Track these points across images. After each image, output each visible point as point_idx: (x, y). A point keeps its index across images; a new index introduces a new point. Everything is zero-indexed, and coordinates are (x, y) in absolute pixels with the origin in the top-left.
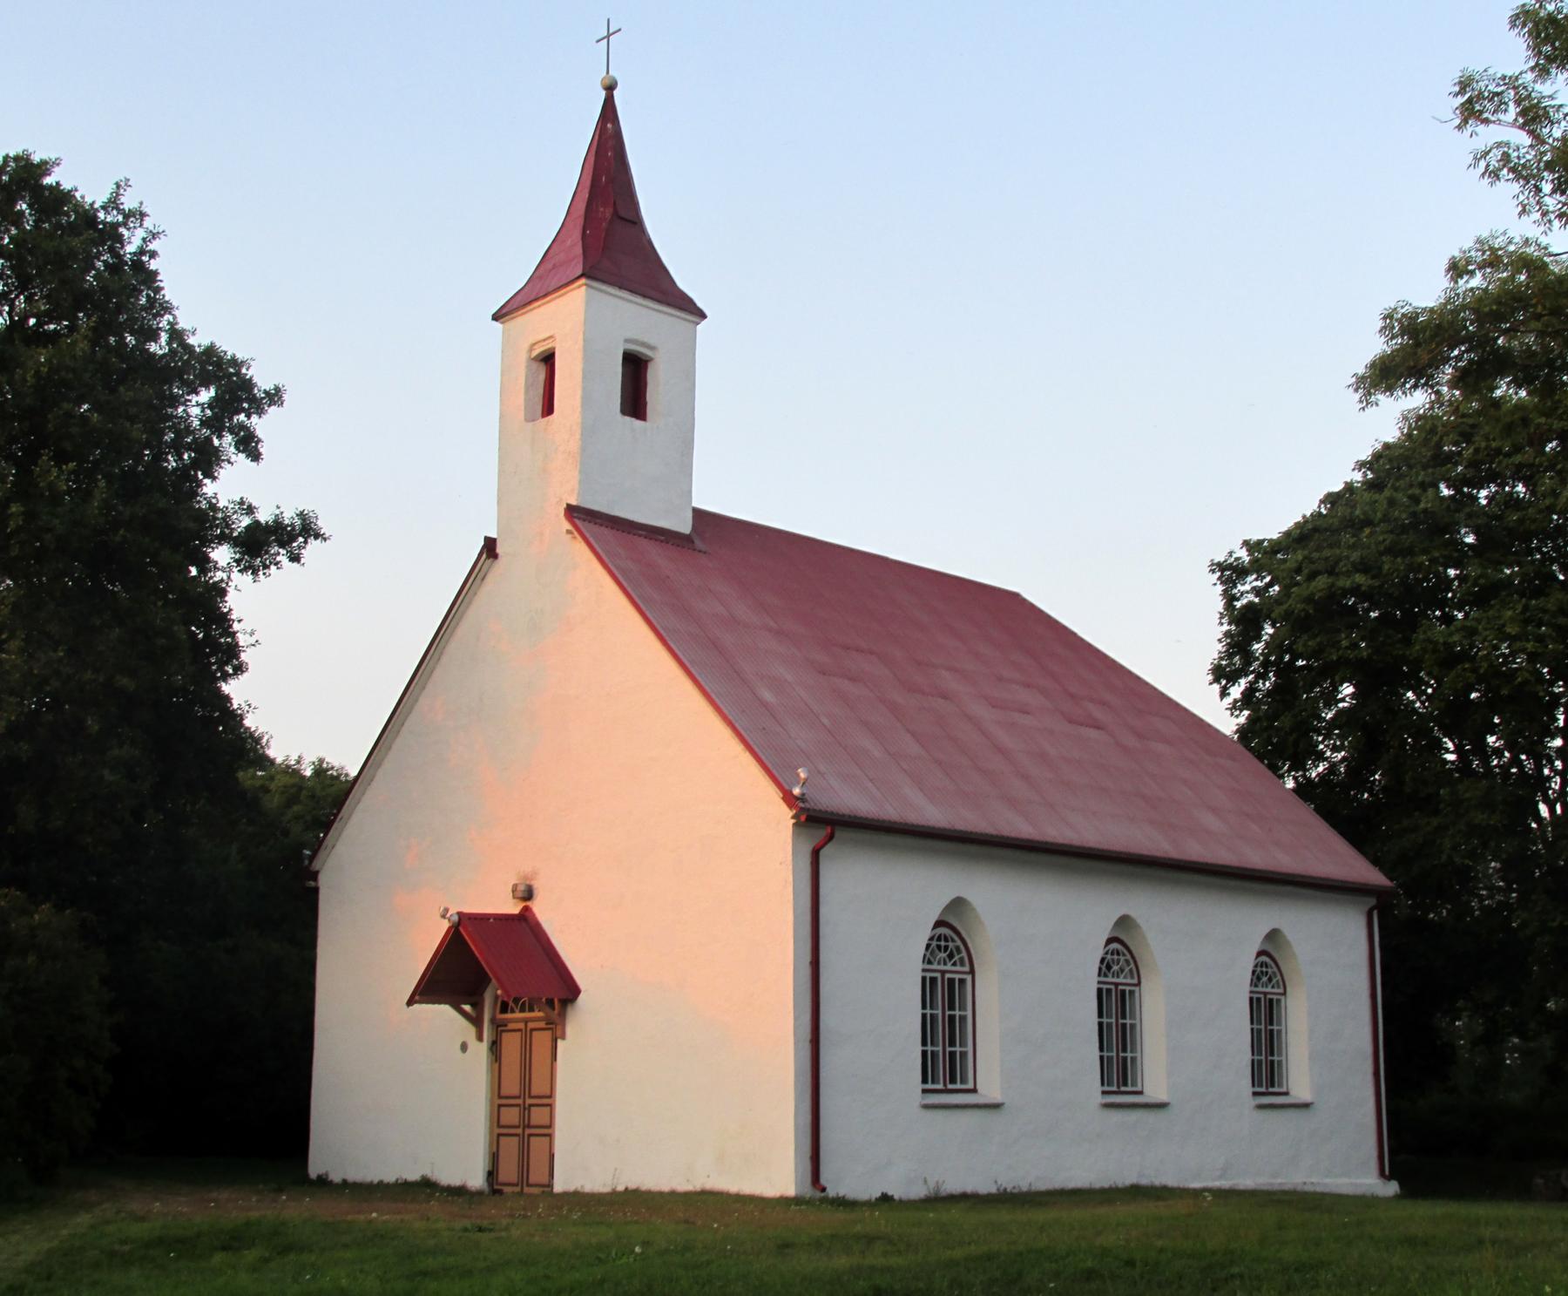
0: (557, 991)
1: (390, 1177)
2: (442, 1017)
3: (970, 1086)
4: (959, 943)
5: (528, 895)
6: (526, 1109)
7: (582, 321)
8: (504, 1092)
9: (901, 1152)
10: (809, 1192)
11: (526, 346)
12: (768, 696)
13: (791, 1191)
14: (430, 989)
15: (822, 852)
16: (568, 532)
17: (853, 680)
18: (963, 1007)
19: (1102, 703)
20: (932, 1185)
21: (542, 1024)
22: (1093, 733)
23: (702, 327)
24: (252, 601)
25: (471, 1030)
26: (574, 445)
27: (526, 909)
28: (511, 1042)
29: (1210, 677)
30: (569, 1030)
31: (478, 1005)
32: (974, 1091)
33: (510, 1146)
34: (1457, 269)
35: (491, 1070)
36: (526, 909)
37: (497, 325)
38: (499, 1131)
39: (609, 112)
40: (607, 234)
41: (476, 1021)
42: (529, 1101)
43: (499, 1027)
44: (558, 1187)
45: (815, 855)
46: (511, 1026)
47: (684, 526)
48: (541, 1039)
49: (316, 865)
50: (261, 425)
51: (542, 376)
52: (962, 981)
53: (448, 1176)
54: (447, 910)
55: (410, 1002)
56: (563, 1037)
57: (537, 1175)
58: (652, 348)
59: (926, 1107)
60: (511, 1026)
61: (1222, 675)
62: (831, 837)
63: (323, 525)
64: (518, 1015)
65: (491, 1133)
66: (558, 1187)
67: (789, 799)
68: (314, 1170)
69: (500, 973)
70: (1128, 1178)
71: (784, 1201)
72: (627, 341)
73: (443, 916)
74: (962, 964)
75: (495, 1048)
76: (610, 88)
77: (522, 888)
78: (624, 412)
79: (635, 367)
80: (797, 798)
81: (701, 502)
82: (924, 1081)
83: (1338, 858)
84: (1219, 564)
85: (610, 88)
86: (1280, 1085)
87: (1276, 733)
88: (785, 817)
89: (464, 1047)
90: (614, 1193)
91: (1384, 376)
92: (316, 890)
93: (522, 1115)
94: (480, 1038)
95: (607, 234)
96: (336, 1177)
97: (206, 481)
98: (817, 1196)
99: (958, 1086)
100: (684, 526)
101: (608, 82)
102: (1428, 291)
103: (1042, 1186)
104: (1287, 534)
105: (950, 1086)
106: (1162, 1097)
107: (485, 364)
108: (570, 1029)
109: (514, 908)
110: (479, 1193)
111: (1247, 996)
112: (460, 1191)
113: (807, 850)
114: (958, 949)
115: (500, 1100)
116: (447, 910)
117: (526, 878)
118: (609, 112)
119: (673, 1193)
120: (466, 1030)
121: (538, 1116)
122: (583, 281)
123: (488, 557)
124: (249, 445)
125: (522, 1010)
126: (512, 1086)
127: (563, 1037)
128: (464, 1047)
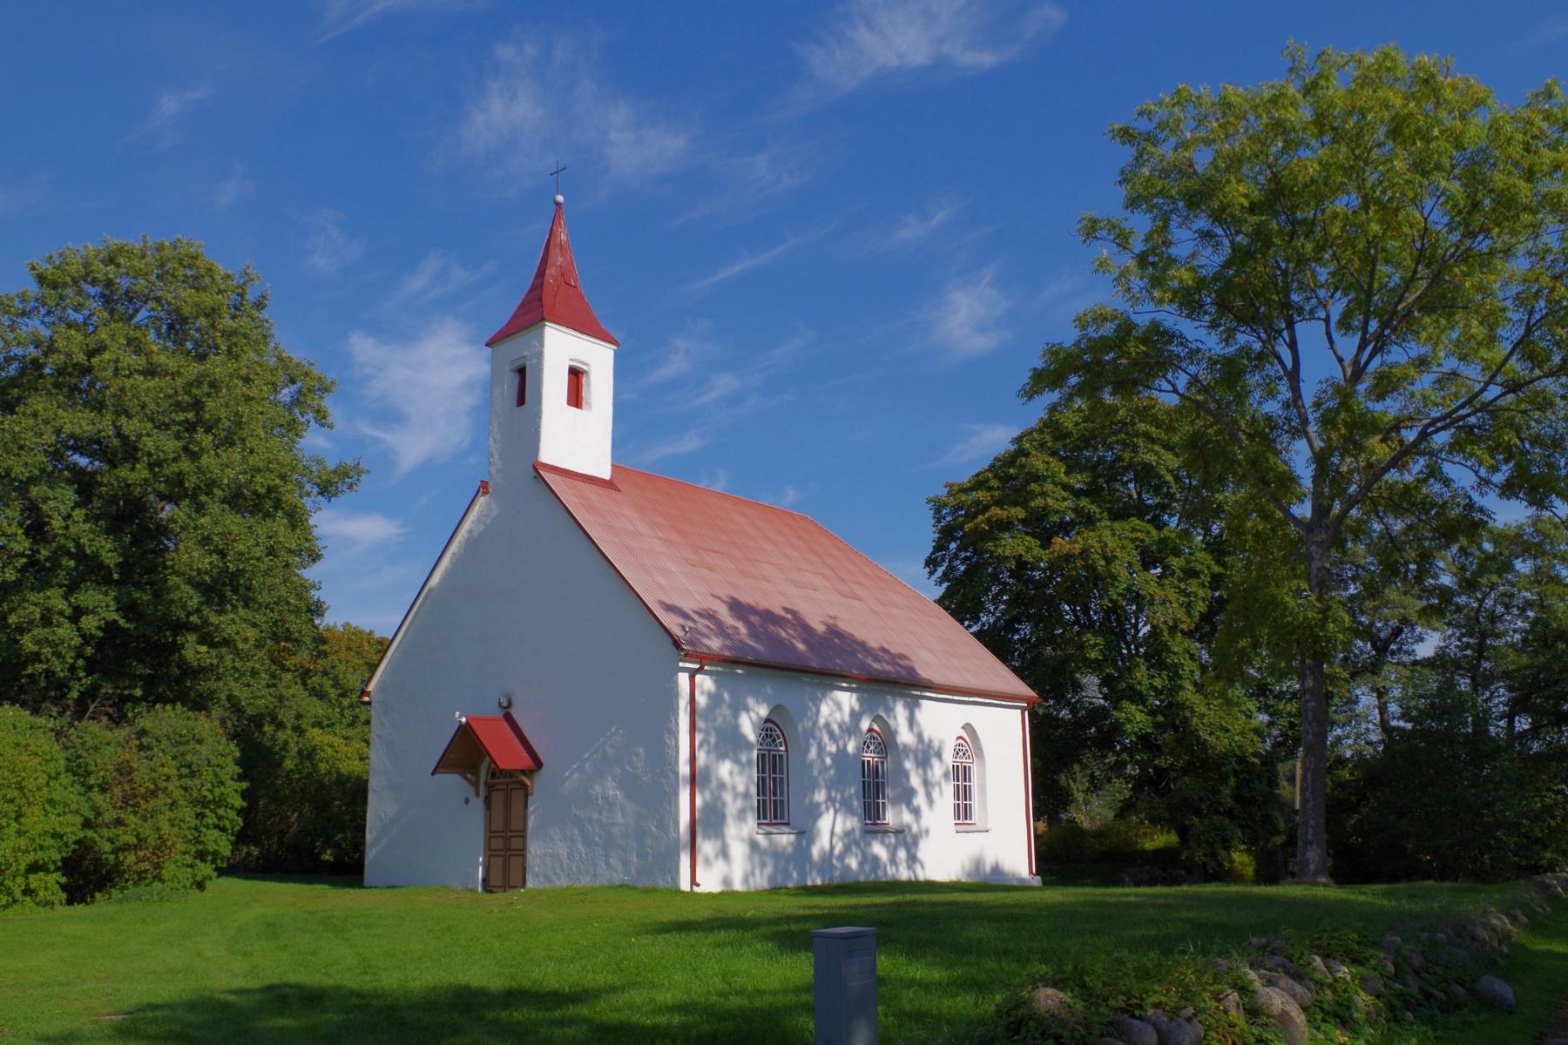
6: (507, 840)
8: (522, 792)
12: (662, 581)
17: (1406, 289)
19: (861, 584)
22: (853, 602)
24: (329, 522)
28: (498, 798)
31: (476, 774)
34: (1082, 323)
37: (489, 350)
41: (476, 785)
50: (327, 402)
51: (517, 381)
78: (569, 403)
83: (1003, 678)
89: (467, 801)
91: (1030, 393)
94: (477, 795)
102: (1069, 337)
121: (515, 843)
124: (321, 417)
126: (498, 824)
128: (467, 801)
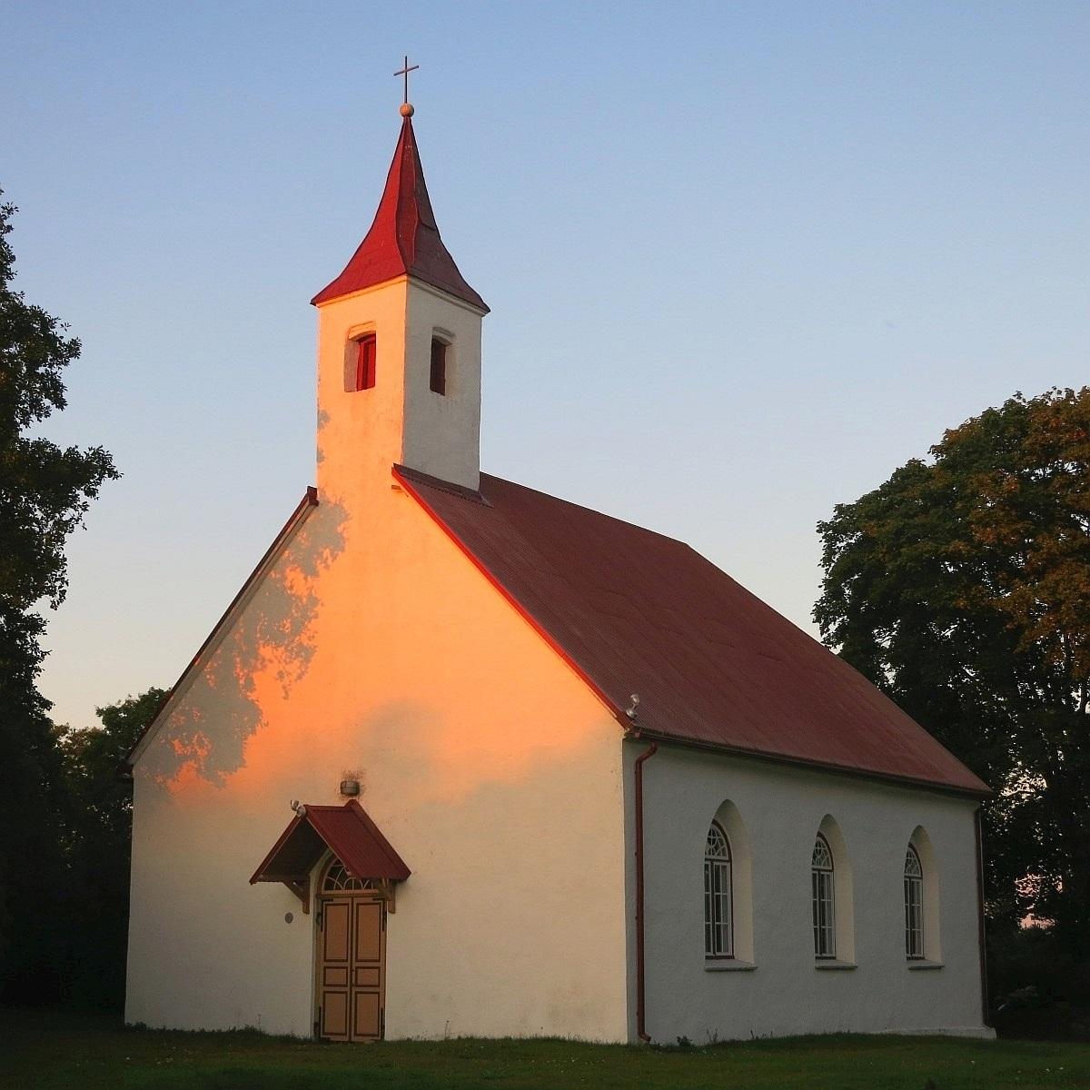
0: (384, 873)
1: (225, 1026)
2: (277, 891)
3: (730, 954)
4: (722, 837)
5: (356, 790)
7: (388, 307)
9: (700, 1011)
10: (636, 1041)
11: (346, 328)
13: (624, 1040)
14: (268, 871)
15: (644, 763)
16: (394, 487)
18: (726, 891)
20: (712, 1033)
21: (370, 900)
23: (486, 319)
25: (299, 905)
26: (398, 413)
27: (352, 802)
28: (337, 916)
29: (814, 617)
30: (399, 905)
32: (732, 957)
33: (337, 1004)
35: (317, 939)
36: (352, 802)
38: (324, 988)
39: (407, 134)
40: (406, 238)
41: (304, 897)
42: (355, 964)
43: (323, 900)
44: (390, 1035)
45: (639, 764)
46: (336, 901)
47: (474, 485)
48: (369, 914)
49: (131, 761)
52: (724, 867)
53: (275, 1025)
54: (297, 803)
55: (252, 881)
56: (393, 912)
57: (366, 1025)
58: (452, 335)
59: (708, 971)
60: (336, 901)
61: (822, 614)
62: (653, 751)
63: (117, 463)
64: (343, 892)
65: (317, 990)
66: (390, 1035)
67: (622, 718)
68: (131, 1017)
69: (337, 858)
70: (833, 1028)
71: (615, 1047)
72: (434, 329)
73: (294, 809)
74: (724, 855)
75: (321, 919)
76: (408, 115)
77: (349, 785)
79: (439, 349)
80: (631, 719)
81: (487, 467)
82: (708, 949)
84: (824, 525)
85: (408, 115)
86: (919, 952)
87: (862, 656)
88: (618, 732)
89: (289, 918)
90: (447, 1041)
92: (131, 781)
93: (351, 973)
94: (306, 911)
95: (406, 238)
96: (153, 1024)
97: (22, 426)
98: (641, 1048)
99: (722, 954)
100: (474, 485)
101: (406, 109)
103: (778, 1034)
104: (866, 500)
105: (718, 954)
106: (851, 961)
107: (317, 339)
108: (400, 905)
109: (339, 802)
110: (306, 1041)
111: (809, 873)
112: (288, 1041)
113: (633, 760)
114: (915, 861)
115: (324, 962)
116: (297, 803)
117: (351, 776)
118: (407, 134)
119: (507, 1040)
120: (296, 906)
122: (405, 277)
123: (310, 504)
125: (348, 887)
126: (338, 949)
127: (393, 912)
128: (289, 918)
